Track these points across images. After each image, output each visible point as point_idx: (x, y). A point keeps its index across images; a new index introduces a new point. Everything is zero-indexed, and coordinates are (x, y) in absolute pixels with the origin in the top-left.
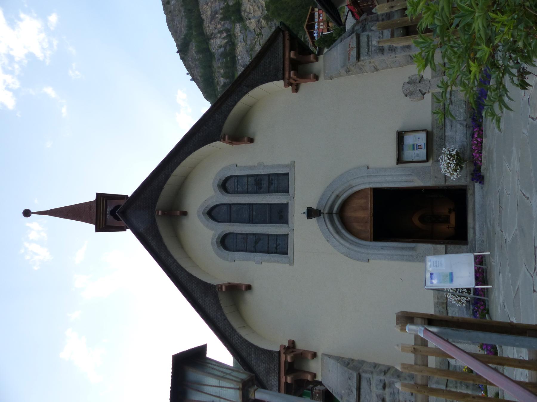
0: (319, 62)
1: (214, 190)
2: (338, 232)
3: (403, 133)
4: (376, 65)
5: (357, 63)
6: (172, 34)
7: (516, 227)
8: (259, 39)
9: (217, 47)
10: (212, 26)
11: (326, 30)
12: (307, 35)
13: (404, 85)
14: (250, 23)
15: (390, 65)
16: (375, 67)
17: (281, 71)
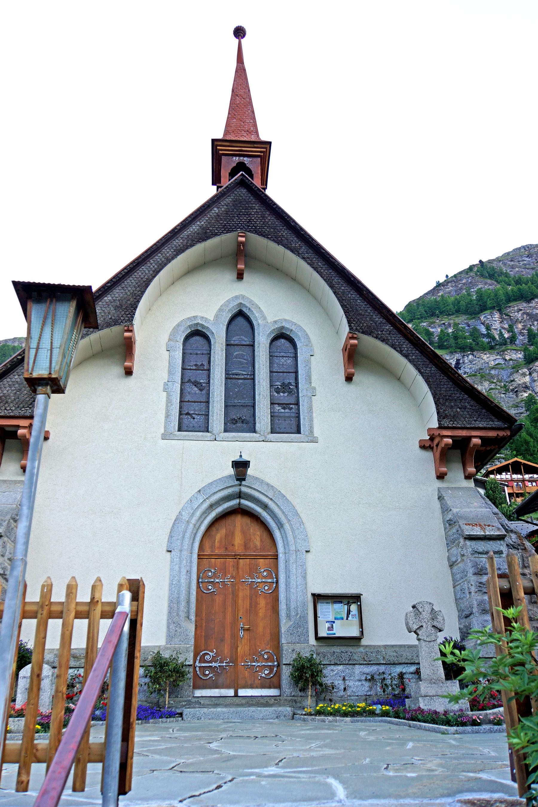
0: (464, 480)
1: (275, 322)
2: (212, 507)
3: (359, 603)
4: (457, 564)
5: (463, 536)
6: (508, 254)
7: (232, 753)
8: (499, 387)
9: (488, 323)
10: (520, 315)
11: (511, 492)
12: (504, 463)
13: (430, 603)
14: (524, 375)
15: (458, 585)
16: (456, 561)
17: (452, 424)
